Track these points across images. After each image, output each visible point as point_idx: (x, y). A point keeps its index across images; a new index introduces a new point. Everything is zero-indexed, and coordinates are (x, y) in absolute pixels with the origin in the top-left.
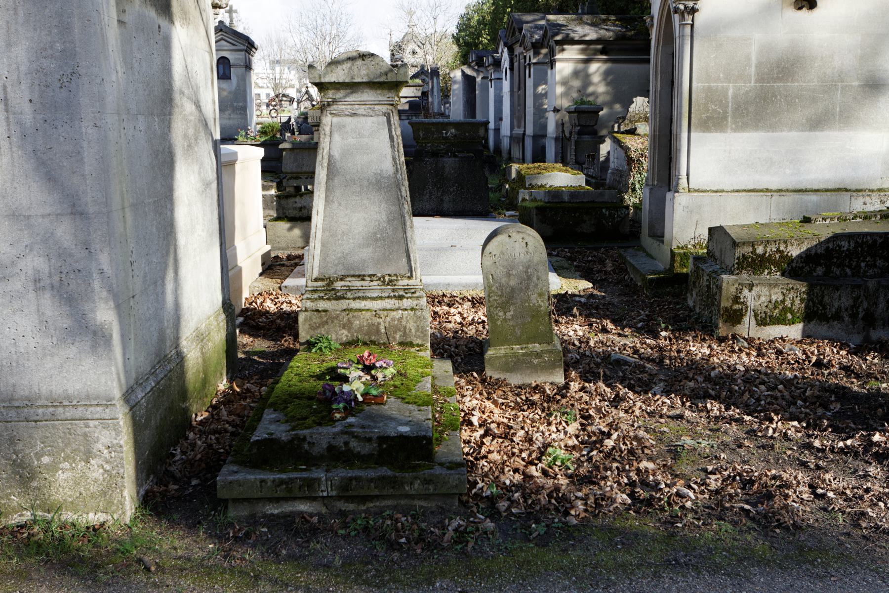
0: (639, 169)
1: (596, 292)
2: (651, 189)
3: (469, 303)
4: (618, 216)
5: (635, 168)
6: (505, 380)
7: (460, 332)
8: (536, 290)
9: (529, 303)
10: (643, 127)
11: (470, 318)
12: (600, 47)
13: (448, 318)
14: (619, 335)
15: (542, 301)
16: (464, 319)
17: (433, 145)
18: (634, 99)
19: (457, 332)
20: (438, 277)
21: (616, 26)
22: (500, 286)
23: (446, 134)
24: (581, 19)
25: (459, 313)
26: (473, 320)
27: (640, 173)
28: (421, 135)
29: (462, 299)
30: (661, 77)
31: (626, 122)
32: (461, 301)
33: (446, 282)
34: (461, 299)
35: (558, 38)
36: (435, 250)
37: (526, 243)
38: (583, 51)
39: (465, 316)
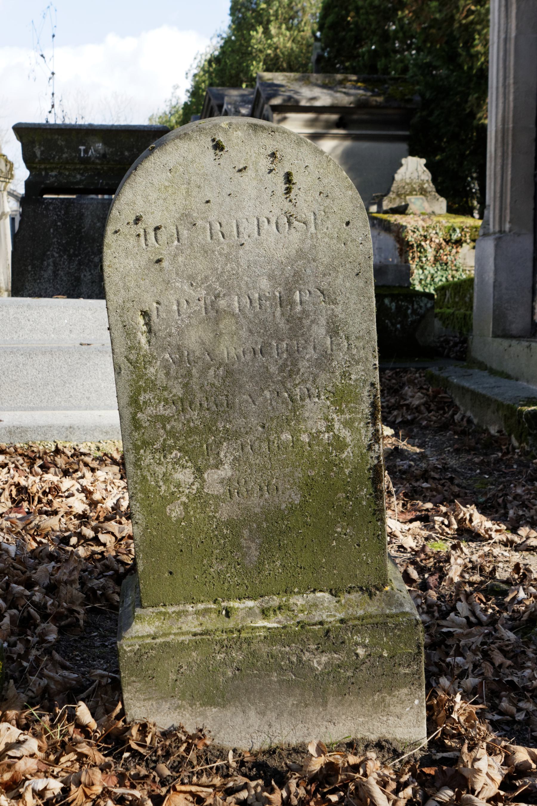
0: (421, 261)
1: (403, 445)
2: (498, 241)
3: (116, 468)
4: (414, 312)
5: (413, 258)
6: (200, 734)
7: (74, 540)
8: (323, 378)
9: (295, 433)
10: (419, 203)
11: (109, 504)
12: (334, 117)
13: (50, 503)
14: (508, 543)
15: (348, 424)
16: (93, 504)
17: (60, 173)
18: (404, 161)
19: (65, 541)
20: (49, 413)
21: (359, 88)
22: (179, 363)
23: (86, 151)
24: (308, 78)
25: (84, 490)
26: (116, 507)
27: (422, 268)
28: (38, 154)
29: (101, 460)
30: (518, 8)
31: (392, 195)
32: (95, 464)
33: (67, 422)
34: (95, 459)
35: (276, 101)
36: (44, 353)
37: (288, 178)
38: (311, 123)
39: (97, 496)
